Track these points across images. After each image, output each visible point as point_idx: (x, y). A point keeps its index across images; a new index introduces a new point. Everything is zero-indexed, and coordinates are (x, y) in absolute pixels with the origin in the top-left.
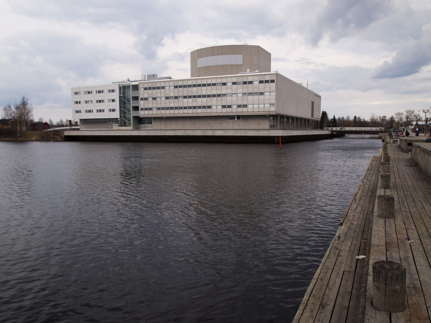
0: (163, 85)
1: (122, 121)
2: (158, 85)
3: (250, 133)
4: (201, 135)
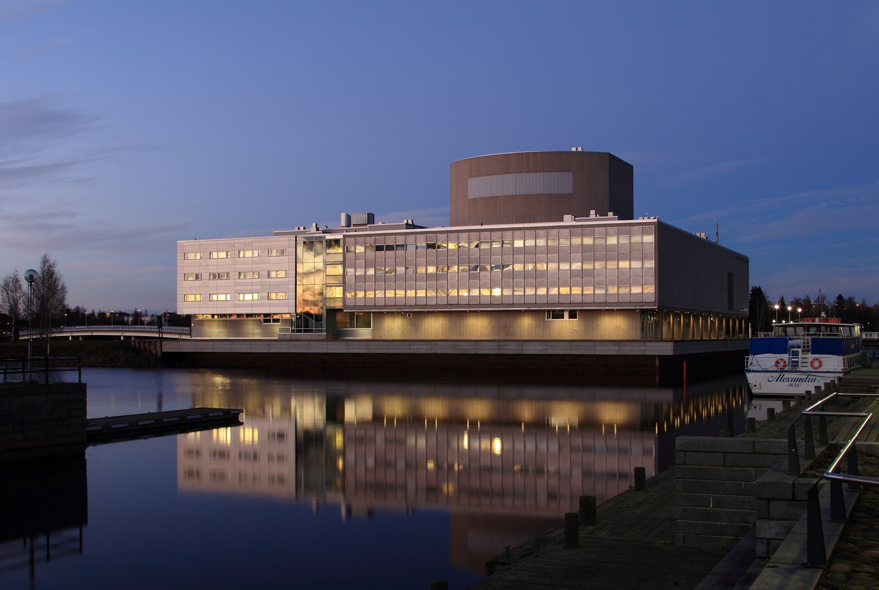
0: (400, 241)
1: (643, 340)
2: (390, 241)
3: (602, 348)
4: (381, 351)
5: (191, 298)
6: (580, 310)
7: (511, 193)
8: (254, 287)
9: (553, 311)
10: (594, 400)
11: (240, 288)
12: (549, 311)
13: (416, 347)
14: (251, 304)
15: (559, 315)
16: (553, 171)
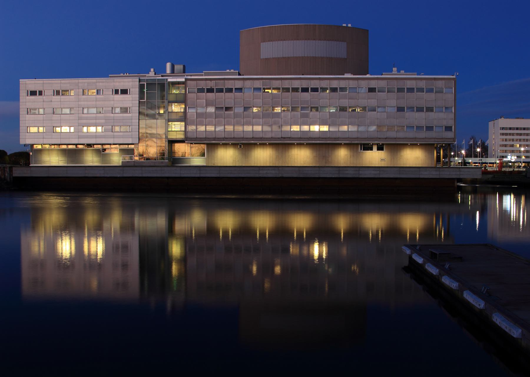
2: (229, 85)
5: (33, 130)
6: (386, 144)
7: (280, 55)
8: (98, 121)
9: (364, 144)
10: (360, 212)
11: (84, 121)
12: (361, 144)
13: (265, 172)
14: (96, 135)
15: (368, 147)
16: (333, 40)
